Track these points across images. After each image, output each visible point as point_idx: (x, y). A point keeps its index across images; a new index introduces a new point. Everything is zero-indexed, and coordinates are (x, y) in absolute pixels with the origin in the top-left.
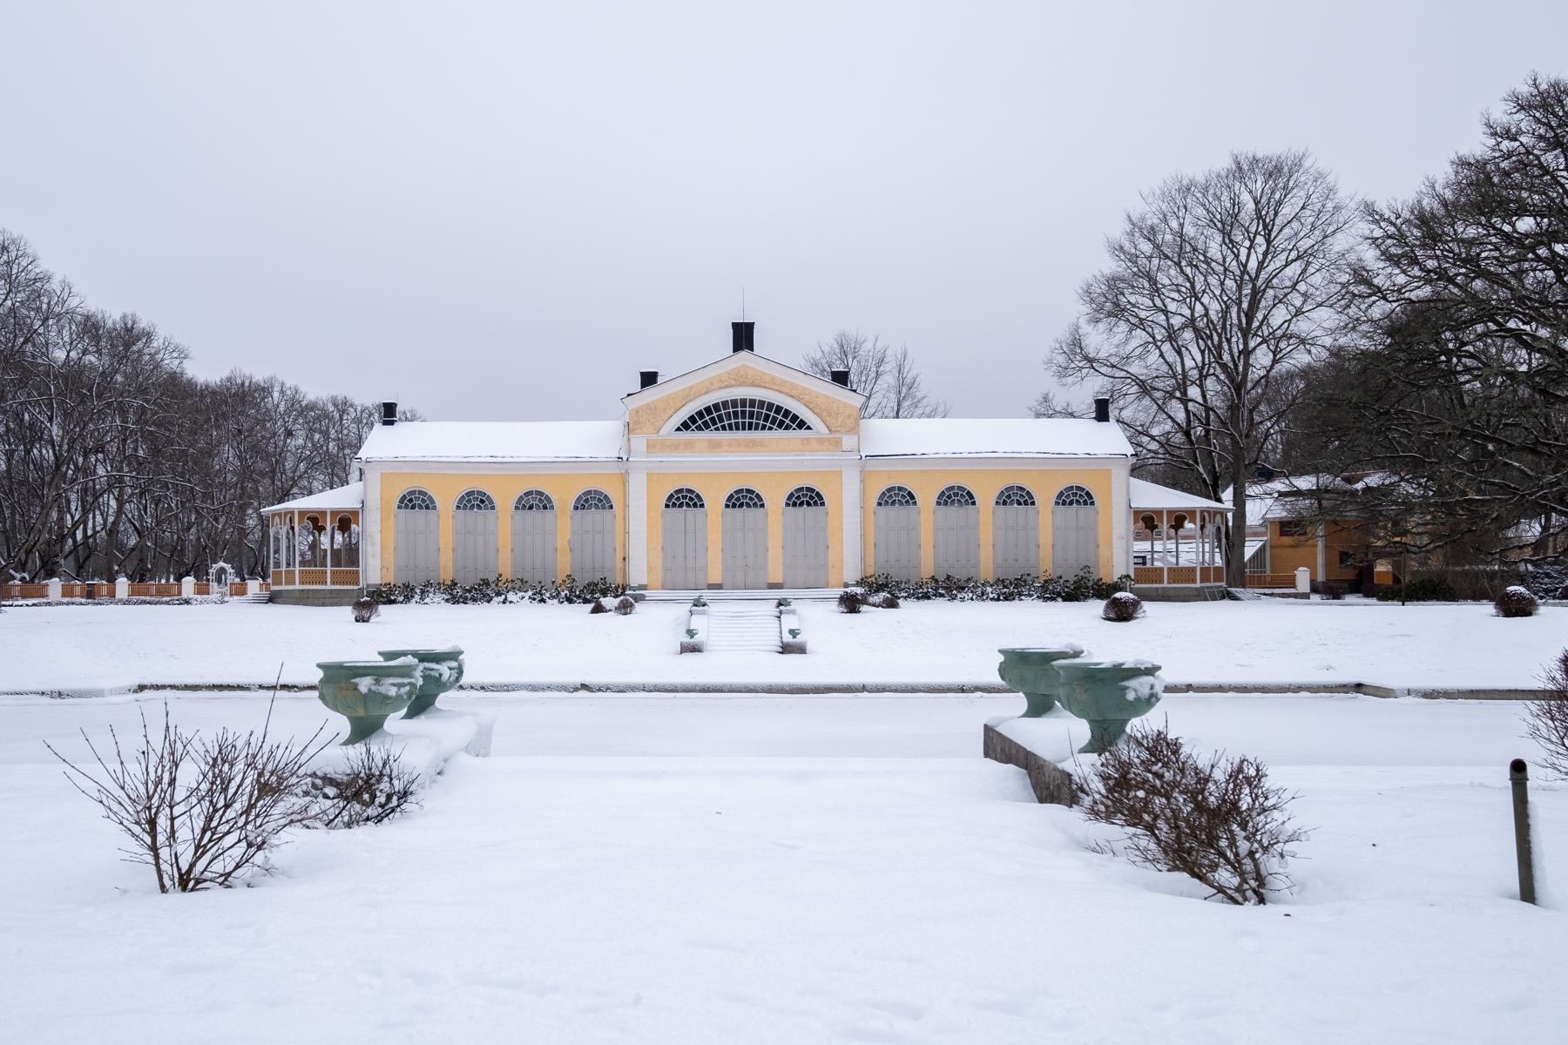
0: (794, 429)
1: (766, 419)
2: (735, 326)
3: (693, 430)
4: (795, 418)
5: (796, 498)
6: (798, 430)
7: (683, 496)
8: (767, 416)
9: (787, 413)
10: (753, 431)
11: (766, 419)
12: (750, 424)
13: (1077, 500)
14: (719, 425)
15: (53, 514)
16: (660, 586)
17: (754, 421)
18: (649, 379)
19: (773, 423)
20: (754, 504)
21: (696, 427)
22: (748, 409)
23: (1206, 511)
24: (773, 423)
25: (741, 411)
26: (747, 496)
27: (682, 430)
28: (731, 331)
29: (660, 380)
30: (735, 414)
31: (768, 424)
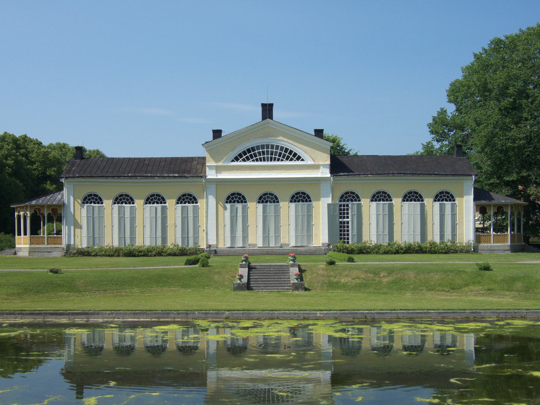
0: (295, 161)
1: (280, 155)
2: (263, 105)
3: (240, 161)
4: (295, 154)
5: (296, 198)
6: (297, 161)
7: (380, 195)
8: (280, 154)
9: (291, 152)
10: (276, 162)
11: (280, 155)
12: (271, 158)
13: (94, 201)
14: (254, 158)
15: (33, 203)
16: (210, 243)
17: (273, 156)
18: (217, 134)
19: (284, 157)
20: (97, 202)
21: (242, 160)
22: (283, 152)
23: (513, 204)
24: (284, 157)
25: (288, 156)
26: (414, 195)
27: (235, 161)
28: (321, 129)
29: (223, 134)
30: (276, 153)
31: (281, 158)
